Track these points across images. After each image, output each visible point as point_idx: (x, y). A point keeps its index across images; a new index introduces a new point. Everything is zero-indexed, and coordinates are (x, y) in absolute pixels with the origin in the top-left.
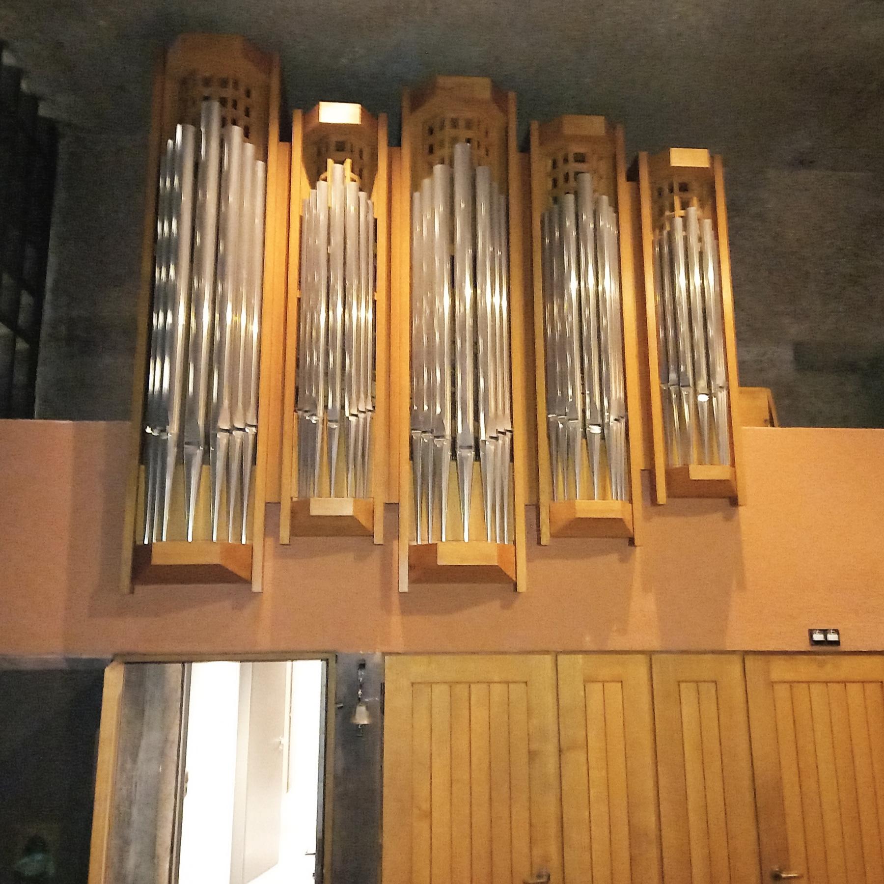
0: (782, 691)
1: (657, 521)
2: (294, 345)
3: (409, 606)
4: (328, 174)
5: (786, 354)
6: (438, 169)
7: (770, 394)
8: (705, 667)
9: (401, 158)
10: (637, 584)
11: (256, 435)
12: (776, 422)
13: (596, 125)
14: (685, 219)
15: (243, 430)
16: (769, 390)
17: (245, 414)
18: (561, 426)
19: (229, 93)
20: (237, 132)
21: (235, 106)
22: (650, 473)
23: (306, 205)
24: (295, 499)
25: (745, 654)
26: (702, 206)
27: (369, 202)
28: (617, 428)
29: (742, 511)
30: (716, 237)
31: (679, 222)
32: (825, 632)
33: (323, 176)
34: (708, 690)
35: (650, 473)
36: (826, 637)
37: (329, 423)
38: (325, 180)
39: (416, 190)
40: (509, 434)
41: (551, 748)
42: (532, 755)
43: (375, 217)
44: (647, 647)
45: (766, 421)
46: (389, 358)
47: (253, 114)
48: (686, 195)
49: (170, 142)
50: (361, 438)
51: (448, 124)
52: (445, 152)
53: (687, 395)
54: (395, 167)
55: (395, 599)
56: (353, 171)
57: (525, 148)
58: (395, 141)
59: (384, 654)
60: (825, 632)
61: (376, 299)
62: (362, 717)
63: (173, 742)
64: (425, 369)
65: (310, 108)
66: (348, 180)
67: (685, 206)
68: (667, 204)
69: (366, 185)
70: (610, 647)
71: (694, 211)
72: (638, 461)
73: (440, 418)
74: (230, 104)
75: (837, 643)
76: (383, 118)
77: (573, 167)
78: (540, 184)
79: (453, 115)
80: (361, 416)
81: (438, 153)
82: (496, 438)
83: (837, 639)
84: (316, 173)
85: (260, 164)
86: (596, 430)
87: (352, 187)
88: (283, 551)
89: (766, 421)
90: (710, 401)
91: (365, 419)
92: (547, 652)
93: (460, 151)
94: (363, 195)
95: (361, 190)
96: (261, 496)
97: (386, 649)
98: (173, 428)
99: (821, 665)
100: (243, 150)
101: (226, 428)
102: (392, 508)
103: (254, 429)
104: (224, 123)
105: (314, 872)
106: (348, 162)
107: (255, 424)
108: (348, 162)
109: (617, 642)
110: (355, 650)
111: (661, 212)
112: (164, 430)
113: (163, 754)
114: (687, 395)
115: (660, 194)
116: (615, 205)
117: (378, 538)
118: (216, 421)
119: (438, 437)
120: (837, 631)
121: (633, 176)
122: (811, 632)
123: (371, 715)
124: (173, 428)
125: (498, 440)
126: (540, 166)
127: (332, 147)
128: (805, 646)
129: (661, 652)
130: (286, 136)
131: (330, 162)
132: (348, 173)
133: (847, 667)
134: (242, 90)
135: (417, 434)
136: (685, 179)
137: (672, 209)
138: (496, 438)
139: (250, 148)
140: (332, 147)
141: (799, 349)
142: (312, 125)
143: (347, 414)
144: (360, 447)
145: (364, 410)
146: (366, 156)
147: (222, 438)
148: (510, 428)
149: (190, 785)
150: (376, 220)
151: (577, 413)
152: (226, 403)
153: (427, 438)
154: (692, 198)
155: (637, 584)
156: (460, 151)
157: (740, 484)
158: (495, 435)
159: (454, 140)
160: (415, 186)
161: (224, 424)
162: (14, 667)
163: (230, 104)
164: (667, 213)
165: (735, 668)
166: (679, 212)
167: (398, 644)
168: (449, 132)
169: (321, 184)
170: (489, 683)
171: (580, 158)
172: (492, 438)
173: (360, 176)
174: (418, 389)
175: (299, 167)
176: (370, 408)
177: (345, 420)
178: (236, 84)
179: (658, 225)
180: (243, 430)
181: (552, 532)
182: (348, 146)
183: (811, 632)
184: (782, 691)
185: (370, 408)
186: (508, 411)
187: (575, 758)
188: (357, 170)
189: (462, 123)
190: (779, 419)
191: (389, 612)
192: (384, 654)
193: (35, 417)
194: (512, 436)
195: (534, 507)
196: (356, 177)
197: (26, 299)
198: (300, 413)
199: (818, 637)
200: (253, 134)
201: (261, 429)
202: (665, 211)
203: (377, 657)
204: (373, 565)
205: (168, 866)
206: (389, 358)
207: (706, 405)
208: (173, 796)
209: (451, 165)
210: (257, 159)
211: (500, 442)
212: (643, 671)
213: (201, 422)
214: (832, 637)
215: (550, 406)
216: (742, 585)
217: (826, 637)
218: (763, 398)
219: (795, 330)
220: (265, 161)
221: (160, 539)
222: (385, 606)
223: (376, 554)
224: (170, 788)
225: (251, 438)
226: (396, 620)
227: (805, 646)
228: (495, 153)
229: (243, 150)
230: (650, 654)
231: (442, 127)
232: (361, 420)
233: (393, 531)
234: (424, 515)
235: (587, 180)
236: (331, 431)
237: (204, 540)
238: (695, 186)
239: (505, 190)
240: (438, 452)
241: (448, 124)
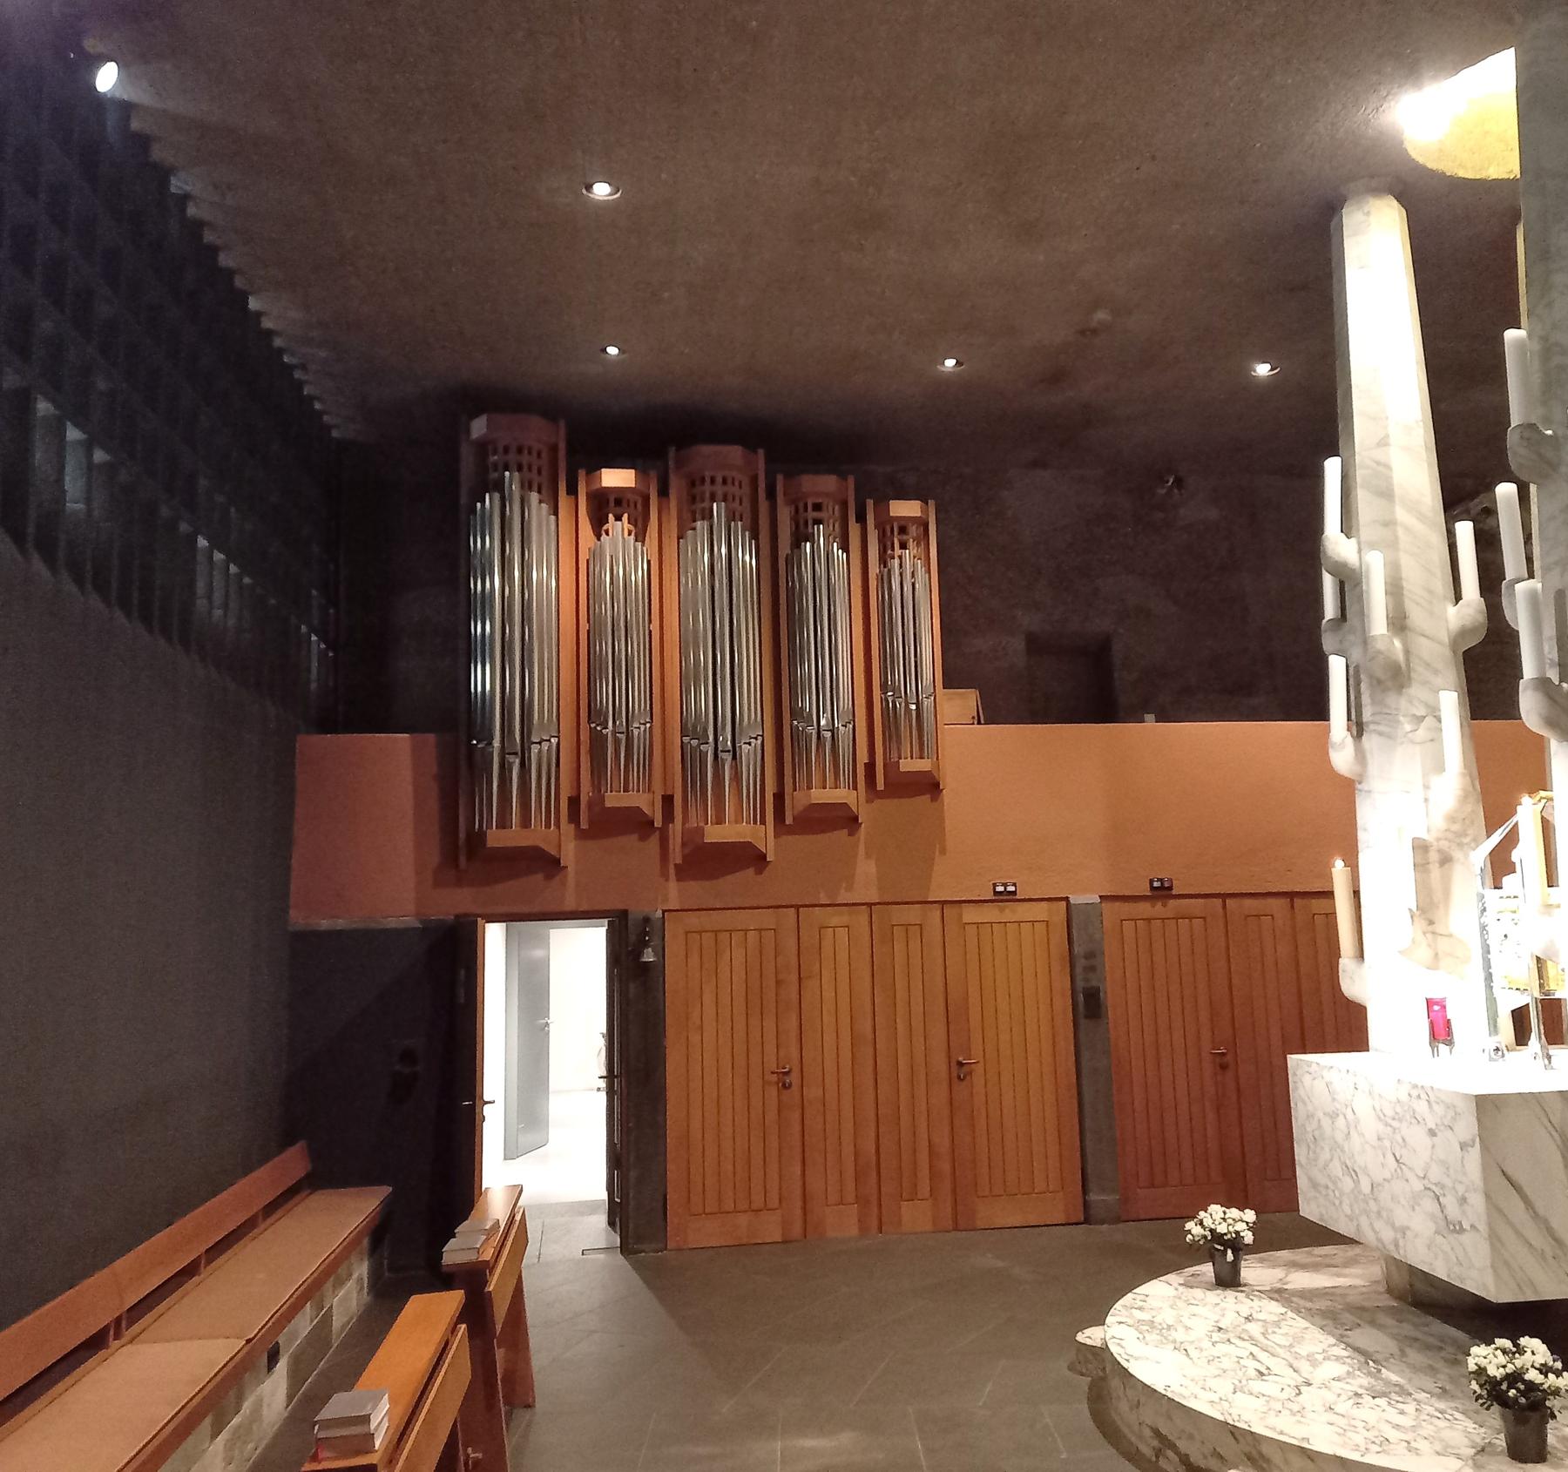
0: (971, 930)
1: (878, 802)
3: (682, 873)
5: (1018, 644)
8: (912, 914)
9: (669, 514)
11: (558, 744)
21: (530, 469)
22: (870, 767)
29: (947, 794)
32: (1005, 885)
35: (870, 767)
39: (682, 538)
44: (867, 900)
46: (662, 680)
47: (544, 473)
49: (479, 505)
54: (664, 519)
55: (672, 871)
56: (629, 523)
57: (771, 494)
58: (663, 492)
59: (664, 912)
60: (1005, 885)
64: (690, 585)
68: (889, 543)
69: (641, 537)
70: (1044, 904)
72: (863, 757)
75: (1014, 893)
76: (653, 474)
78: (785, 515)
79: (712, 473)
84: (598, 525)
88: (581, 835)
92: (792, 906)
98: (496, 743)
99: (1002, 910)
100: (539, 509)
102: (668, 800)
103: (557, 739)
110: (637, 911)
111: (885, 551)
115: (391, 1461)
118: (529, 737)
120: (1014, 885)
121: (861, 519)
123: (656, 955)
126: (785, 515)
127: (612, 504)
129: (879, 903)
130: (572, 490)
135: (686, 739)
136: (903, 523)
137: (893, 550)
148: (761, 733)
153: (695, 742)
164: (889, 552)
165: (936, 913)
166: (898, 552)
168: (707, 488)
170: (747, 930)
174: (686, 673)
179: (883, 561)
183: (995, 885)
184: (971, 930)
188: (632, 520)
191: (667, 880)
195: (779, 797)
199: (1000, 889)
203: (659, 914)
206: (662, 680)
214: (1011, 889)
216: (943, 851)
217: (1005, 889)
219: (1029, 621)
226: (673, 887)
227: (990, 896)
229: (539, 509)
230: (870, 905)
233: (668, 815)
234: (694, 804)
237: (954, 1014)
240: (703, 755)
241: (708, 480)
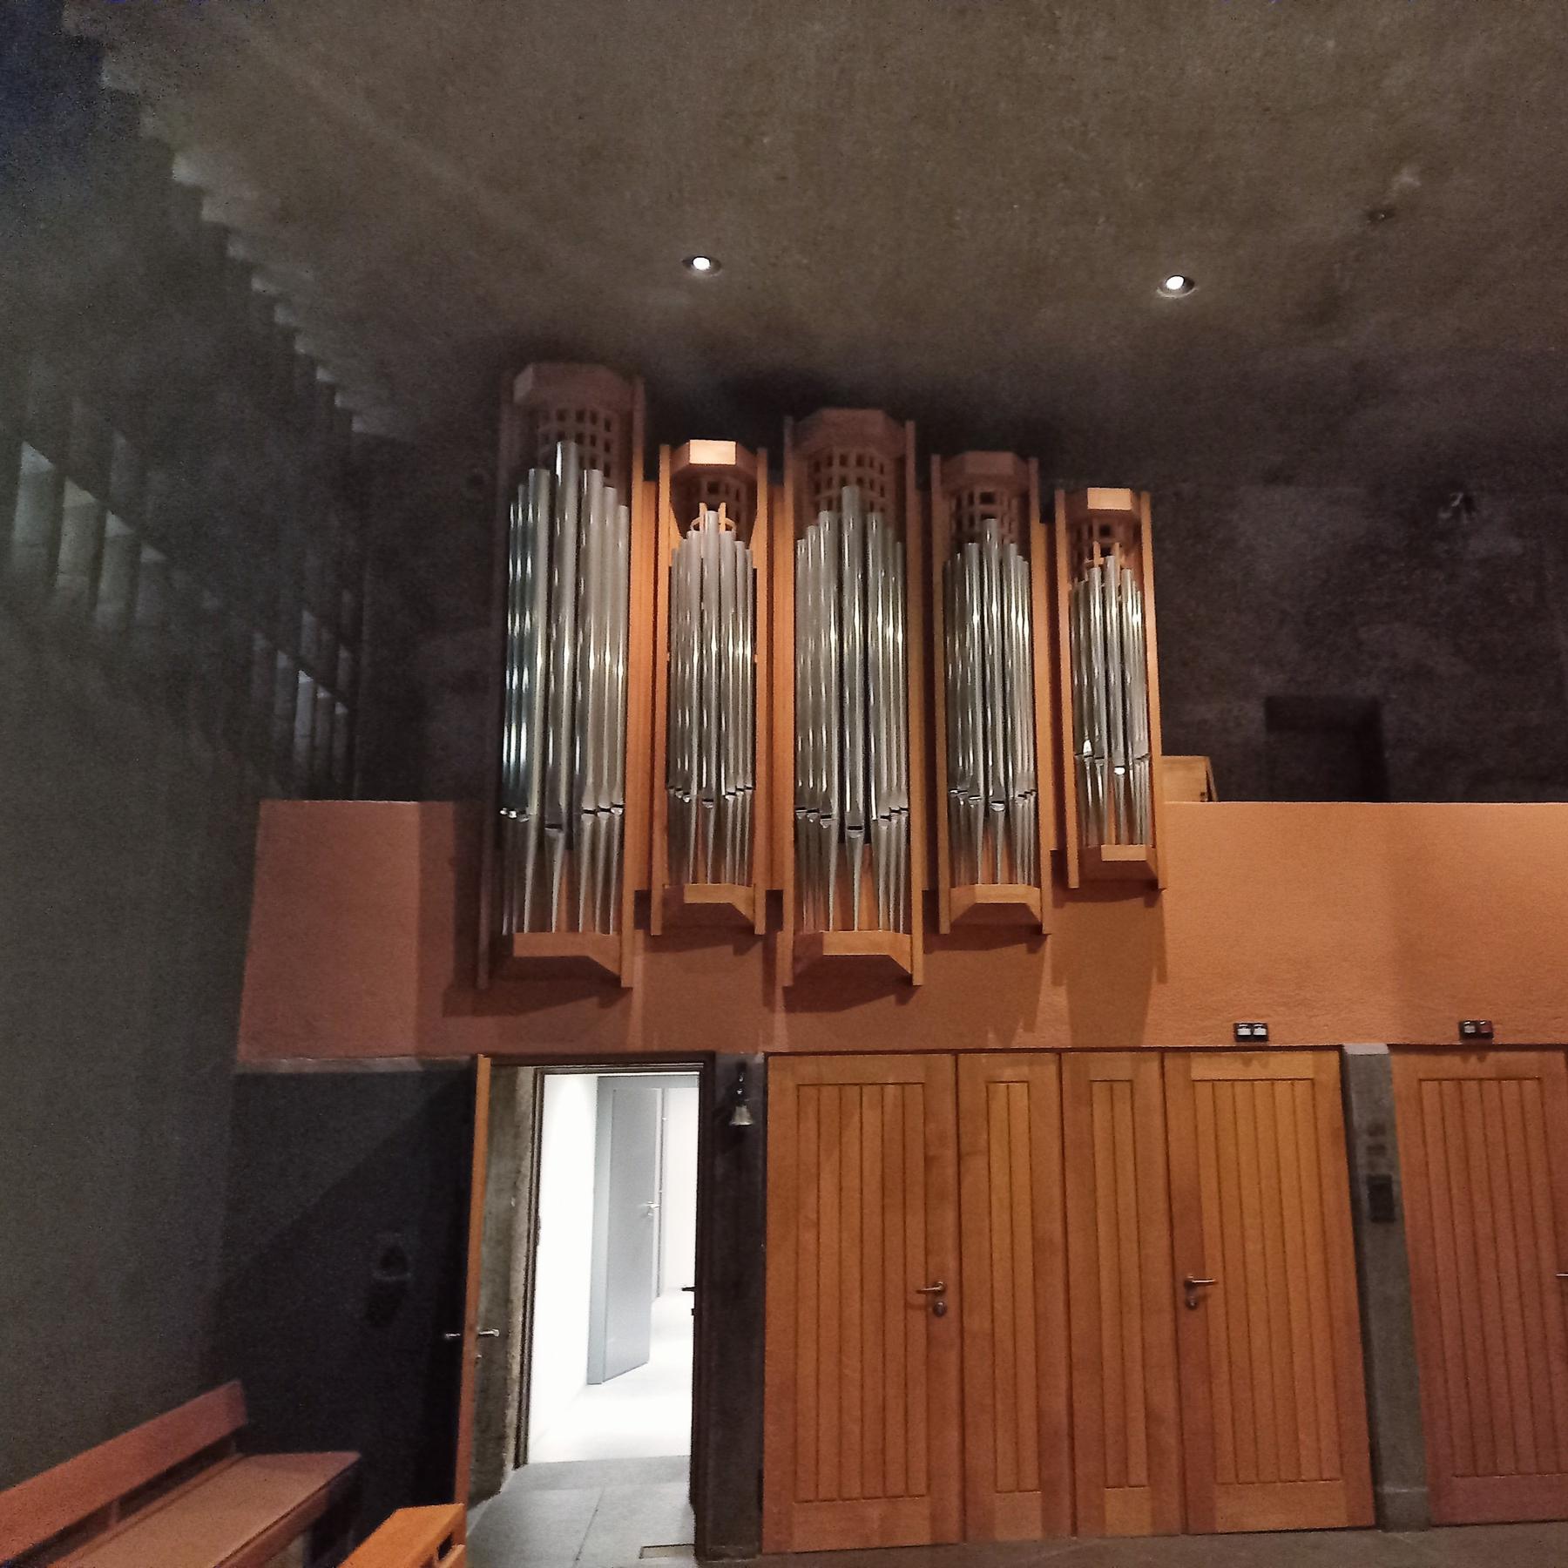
0: (1204, 1091)
2: (664, 723)
3: (797, 1000)
4: (700, 520)
5: (1254, 712)
6: (825, 516)
7: (1209, 764)
8: (1121, 1065)
9: (782, 496)
10: (1047, 976)
11: (623, 816)
12: (1214, 796)
13: (1003, 462)
14: (1103, 568)
15: (609, 810)
16: (1208, 758)
17: (610, 795)
18: (962, 803)
19: (587, 428)
20: (597, 475)
21: (593, 442)
22: (1059, 857)
23: (679, 557)
24: (666, 887)
25: (1163, 1051)
26: (1127, 553)
27: (747, 551)
28: (1024, 806)
29: (1167, 897)
30: (1141, 587)
31: (1096, 572)
32: (1251, 1026)
33: (694, 523)
34: (1122, 1090)
35: (1059, 857)
36: (1252, 1032)
37: (704, 803)
38: (697, 528)
40: (1034, 793)
41: (950, 1154)
42: (928, 1161)
43: (755, 567)
45: (1202, 794)
48: (1107, 541)
50: (739, 819)
51: (836, 461)
52: (833, 493)
53: (1102, 767)
54: (777, 506)
57: (924, 486)
58: (776, 479)
59: (767, 1055)
60: (1251, 1026)
61: (756, 661)
62: (743, 1119)
63: (525, 1176)
65: (678, 441)
66: (723, 527)
67: (1106, 552)
68: (1086, 550)
69: (744, 533)
71: (1113, 562)
72: (1049, 843)
73: (827, 797)
74: (587, 441)
77: (979, 508)
80: (740, 794)
81: (825, 493)
82: (889, 818)
83: (1264, 1034)
84: (686, 519)
85: (623, 509)
86: (999, 808)
87: (728, 536)
88: (655, 945)
89: (1202, 794)
90: (1127, 774)
91: (744, 796)
93: (849, 495)
94: (740, 544)
95: (738, 539)
96: (631, 884)
97: (770, 1049)
98: (533, 809)
100: (603, 495)
101: (591, 809)
102: (775, 898)
103: (621, 811)
104: (581, 466)
105: (693, 1307)
106: (723, 507)
107: (621, 803)
108: (723, 507)
109: (1022, 1039)
111: (1081, 559)
112: (522, 812)
113: (515, 1187)
114: (1102, 767)
116: (1026, 552)
117: (760, 929)
118: (580, 800)
119: (823, 817)
120: (1265, 1026)
121: (1048, 517)
122: (1236, 1027)
123: (753, 1116)
124: (533, 809)
125: (890, 820)
128: (1229, 1042)
130: (651, 475)
131: (702, 506)
132: (723, 520)
133: (1280, 1065)
134: (601, 423)
135: (801, 814)
136: (1106, 522)
137: (1091, 557)
138: (889, 818)
139: (611, 492)
140: (705, 487)
141: (1273, 708)
142: (682, 465)
143: (723, 793)
144: (739, 829)
145: (742, 787)
146: (743, 496)
147: (587, 820)
149: (543, 1233)
150: (755, 571)
151: (979, 789)
152: (590, 780)
153: (812, 817)
154: (1113, 544)
155: (1047, 976)
156: (849, 495)
157: (1160, 864)
158: (887, 814)
159: (844, 482)
160: (800, 534)
161: (588, 805)
162: (366, 1070)
163: (587, 441)
164: (1087, 561)
166: (1098, 560)
167: (780, 1045)
168: (836, 470)
169: (692, 533)
171: (987, 498)
172: (883, 817)
173: (737, 521)
175: (667, 510)
176: (750, 785)
177: (722, 799)
178: (594, 419)
179: (1078, 571)
180: (609, 810)
181: (952, 920)
182: (722, 488)
183: (1236, 1027)
185: (750, 785)
186: (904, 787)
187: (976, 1164)
189: (852, 461)
190: (1218, 795)
191: (773, 1011)
192: (767, 1055)
193: (999, 881)
194: (1037, 794)
195: (931, 897)
196: (731, 522)
197: (344, 654)
198: (672, 791)
199: (1245, 1032)
200: (614, 471)
201: (629, 810)
202: (1084, 559)
203: (759, 1058)
204: (754, 958)
205: (521, 1319)
207: (1122, 780)
208: (526, 1240)
209: (840, 509)
210: (619, 502)
211: (894, 821)
212: (1053, 1068)
213: (563, 802)
214: (1260, 1032)
215: (952, 781)
216: (1163, 978)
217: (1252, 1032)
218: (1197, 769)
219: (1271, 682)
220: (629, 505)
221: (520, 929)
222: (768, 1002)
223: (757, 949)
224: (522, 1227)
225: (617, 819)
226: (780, 1018)
227: (1229, 1042)
228: (889, 500)
229: (603, 495)
230: (1059, 1052)
231: (830, 464)
232: (740, 799)
235: (992, 529)
236: (707, 811)
238: (1120, 531)
239: (901, 536)
